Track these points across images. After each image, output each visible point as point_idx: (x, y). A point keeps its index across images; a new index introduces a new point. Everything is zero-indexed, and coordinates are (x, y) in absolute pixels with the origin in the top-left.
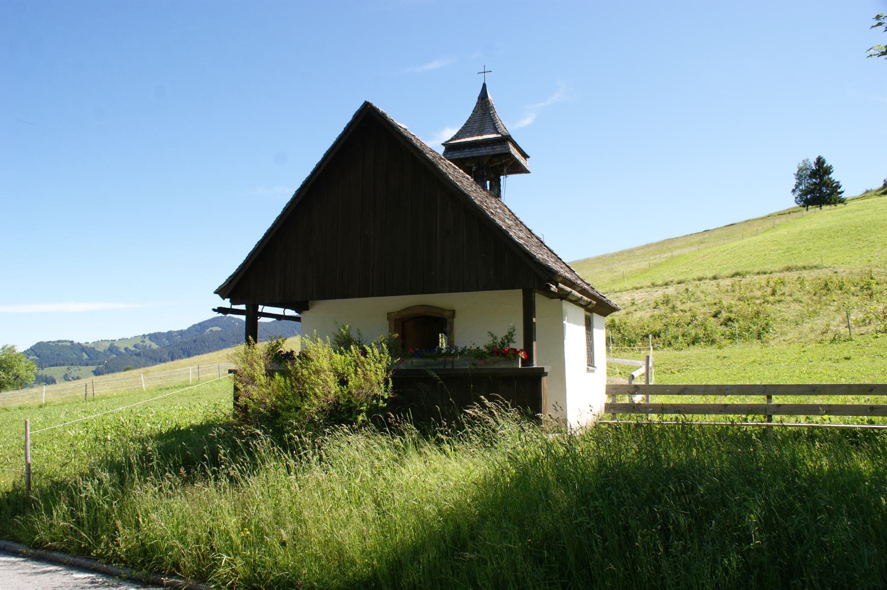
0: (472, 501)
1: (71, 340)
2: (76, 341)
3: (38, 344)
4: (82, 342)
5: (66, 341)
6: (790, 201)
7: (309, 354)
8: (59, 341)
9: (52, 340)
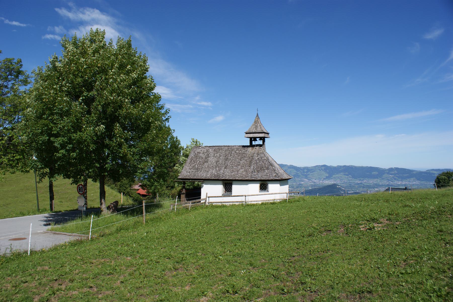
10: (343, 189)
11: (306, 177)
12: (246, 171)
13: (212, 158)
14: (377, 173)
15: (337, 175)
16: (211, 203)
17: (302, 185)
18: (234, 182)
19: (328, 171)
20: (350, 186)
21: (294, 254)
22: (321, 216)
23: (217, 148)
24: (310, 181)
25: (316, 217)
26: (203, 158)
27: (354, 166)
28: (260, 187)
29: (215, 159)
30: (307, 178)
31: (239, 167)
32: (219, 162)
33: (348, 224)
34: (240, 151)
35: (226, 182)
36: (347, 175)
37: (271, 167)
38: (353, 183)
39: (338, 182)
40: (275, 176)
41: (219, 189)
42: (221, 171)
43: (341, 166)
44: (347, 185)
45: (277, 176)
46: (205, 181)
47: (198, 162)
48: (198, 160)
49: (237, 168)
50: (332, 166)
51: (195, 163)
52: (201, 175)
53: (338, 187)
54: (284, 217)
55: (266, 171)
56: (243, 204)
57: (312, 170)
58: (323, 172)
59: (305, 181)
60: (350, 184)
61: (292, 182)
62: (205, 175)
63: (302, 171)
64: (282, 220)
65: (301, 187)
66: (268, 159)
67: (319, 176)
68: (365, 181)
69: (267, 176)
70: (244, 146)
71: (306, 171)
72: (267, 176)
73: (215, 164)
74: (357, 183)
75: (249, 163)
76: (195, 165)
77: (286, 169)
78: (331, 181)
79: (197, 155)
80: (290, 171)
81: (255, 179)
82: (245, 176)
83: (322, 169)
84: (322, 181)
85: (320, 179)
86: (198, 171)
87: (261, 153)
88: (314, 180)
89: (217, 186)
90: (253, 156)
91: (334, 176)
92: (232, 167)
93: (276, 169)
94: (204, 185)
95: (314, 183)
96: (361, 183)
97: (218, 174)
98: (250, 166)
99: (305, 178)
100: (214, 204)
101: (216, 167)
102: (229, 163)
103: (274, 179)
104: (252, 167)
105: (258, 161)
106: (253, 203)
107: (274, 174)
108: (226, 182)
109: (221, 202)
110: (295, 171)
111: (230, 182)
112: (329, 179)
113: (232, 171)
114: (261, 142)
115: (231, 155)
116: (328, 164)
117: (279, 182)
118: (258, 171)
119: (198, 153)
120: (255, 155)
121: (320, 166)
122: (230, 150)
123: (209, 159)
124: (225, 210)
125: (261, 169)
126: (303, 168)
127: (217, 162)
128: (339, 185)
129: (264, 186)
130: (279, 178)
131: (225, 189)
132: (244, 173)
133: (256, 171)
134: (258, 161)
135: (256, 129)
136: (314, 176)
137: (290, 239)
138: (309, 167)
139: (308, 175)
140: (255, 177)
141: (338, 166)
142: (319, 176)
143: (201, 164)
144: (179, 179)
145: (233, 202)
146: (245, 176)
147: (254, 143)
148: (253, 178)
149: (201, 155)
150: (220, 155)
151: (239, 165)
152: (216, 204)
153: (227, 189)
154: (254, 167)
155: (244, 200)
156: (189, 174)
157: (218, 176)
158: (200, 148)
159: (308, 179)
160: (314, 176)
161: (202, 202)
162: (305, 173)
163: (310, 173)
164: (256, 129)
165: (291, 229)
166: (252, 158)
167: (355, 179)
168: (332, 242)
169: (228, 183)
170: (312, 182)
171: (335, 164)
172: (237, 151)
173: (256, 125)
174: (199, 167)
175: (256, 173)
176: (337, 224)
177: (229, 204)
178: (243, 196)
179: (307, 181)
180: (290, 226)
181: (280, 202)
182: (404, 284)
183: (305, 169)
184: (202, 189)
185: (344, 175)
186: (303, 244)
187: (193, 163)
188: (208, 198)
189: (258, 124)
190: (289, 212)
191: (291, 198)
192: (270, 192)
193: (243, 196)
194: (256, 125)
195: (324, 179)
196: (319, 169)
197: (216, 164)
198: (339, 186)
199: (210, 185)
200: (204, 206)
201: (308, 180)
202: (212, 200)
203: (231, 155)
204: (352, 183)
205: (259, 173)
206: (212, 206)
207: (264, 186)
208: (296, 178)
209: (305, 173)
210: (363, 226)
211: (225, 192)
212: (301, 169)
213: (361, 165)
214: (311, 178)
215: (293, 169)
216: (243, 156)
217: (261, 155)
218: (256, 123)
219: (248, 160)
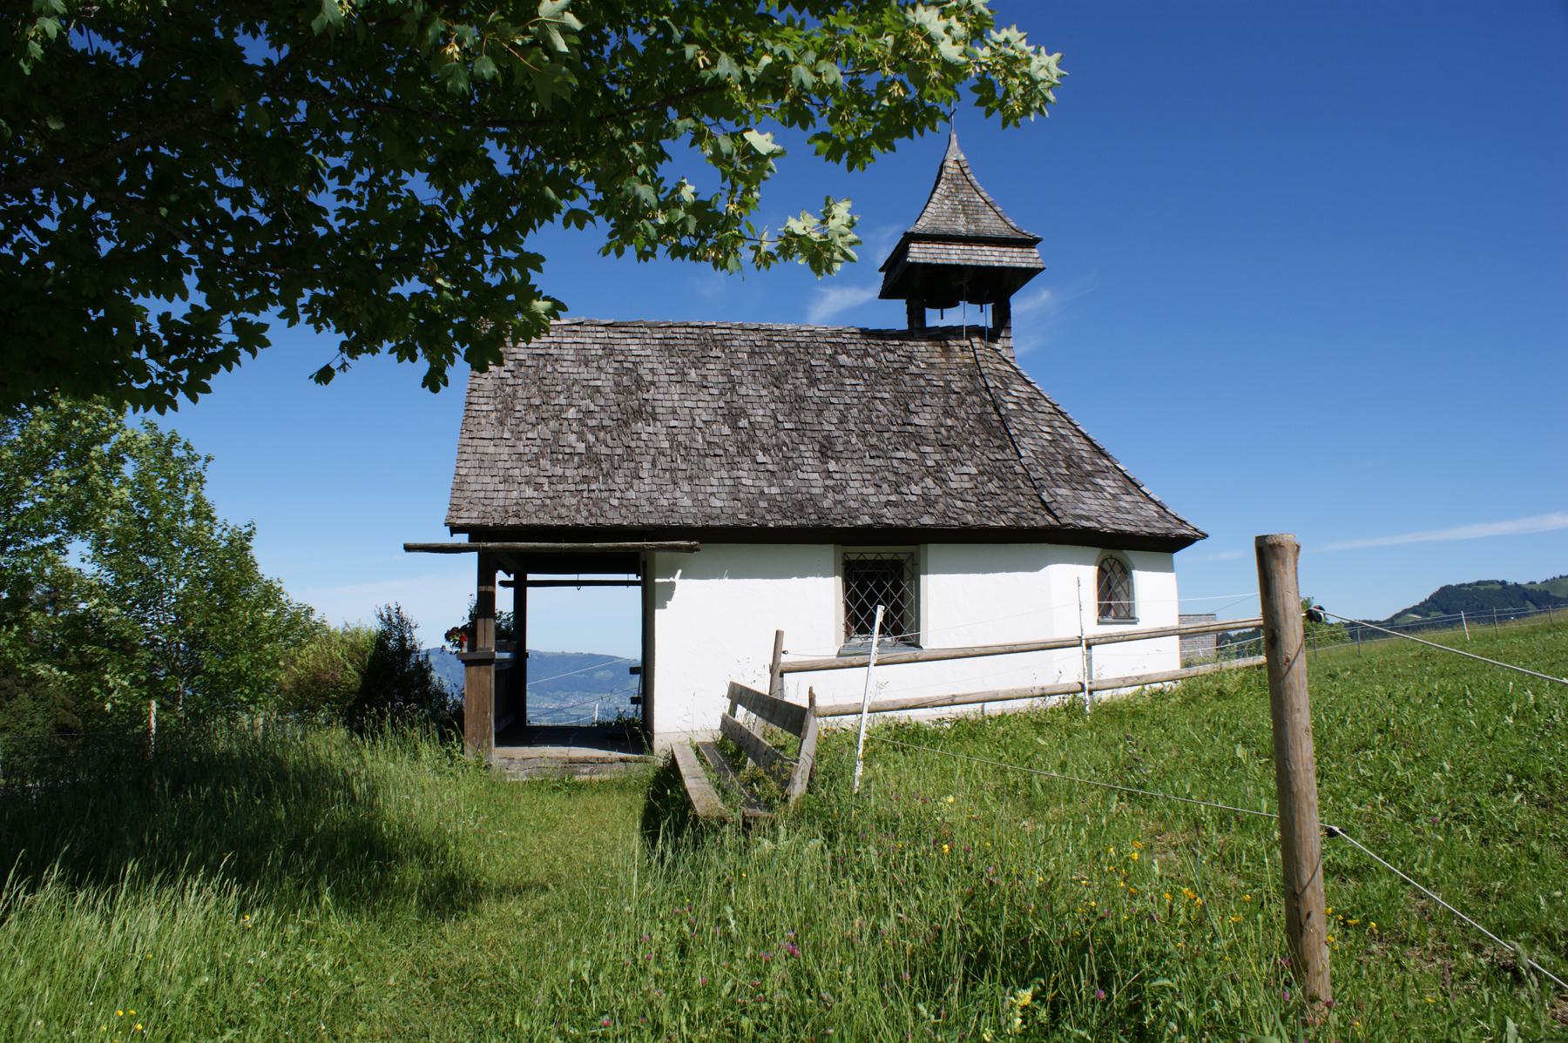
0: (965, 905)
1: (1500, 579)
2: (1511, 580)
3: (1443, 589)
4: (1523, 581)
5: (1492, 582)
6: (1304, 595)
7: (1298, 715)
8: (1479, 583)
9: (1467, 582)
14: (611, 675)
18: (933, 552)
35: (871, 553)
46: (710, 552)
68: (572, 702)
94: (677, 579)
96: (560, 710)
108: (871, 553)
111: (887, 552)
145: (952, 702)
192: (1143, 625)
199: (733, 576)
213: (559, 651)
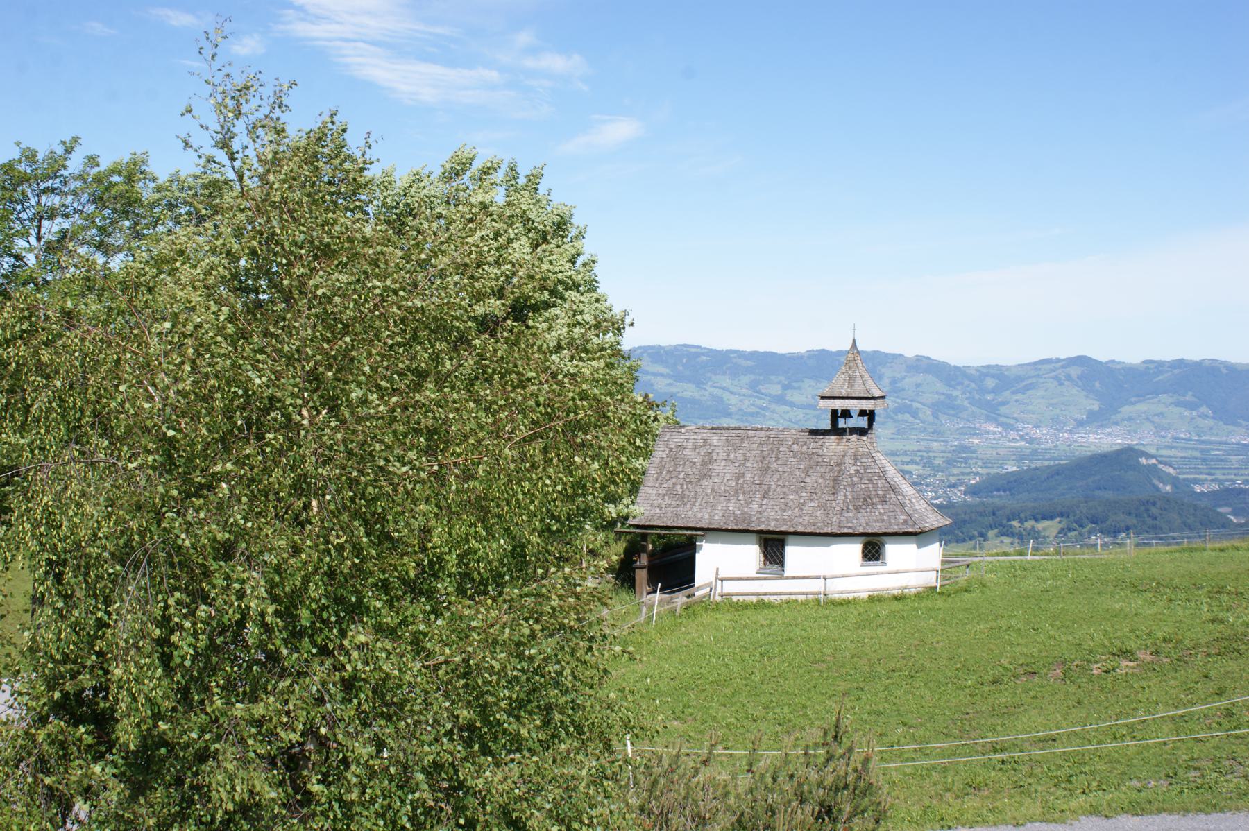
10: (1171, 470)
11: (992, 411)
12: (824, 507)
13: (723, 464)
15: (1142, 407)
16: (728, 594)
17: (974, 452)
18: (790, 539)
19: (1097, 384)
20: (1204, 460)
21: (968, 711)
22: (1020, 641)
23: (733, 433)
24: (1012, 434)
25: (1011, 644)
26: (694, 463)
27: (1222, 362)
28: (863, 552)
29: (731, 467)
30: (996, 420)
31: (804, 494)
32: (743, 476)
33: (1072, 661)
34: (802, 446)
35: (765, 536)
36: (1192, 406)
37: (893, 495)
38: (1220, 443)
39: (1145, 439)
40: (906, 522)
41: (749, 554)
42: (751, 506)
43: (1160, 364)
44: (1189, 453)
45: (911, 523)
46: (709, 534)
47: (682, 475)
48: (680, 469)
49: (797, 497)
50: (1119, 363)
51: (674, 480)
52: (695, 516)
53: (1143, 461)
54: (938, 642)
55: (880, 507)
56: (818, 601)
57: (1019, 379)
58: (1074, 391)
59: (988, 432)
60: (1202, 451)
61: (922, 436)
62: (707, 516)
63: (973, 385)
64: (935, 649)
65: (965, 461)
66: (884, 473)
67: (1058, 411)
69: (883, 521)
70: (814, 432)
71: (990, 383)
72: (883, 521)
73: (734, 484)
74: (1238, 444)
75: (831, 484)
76: (674, 484)
77: (899, 376)
78: (1110, 434)
79: (677, 452)
80: (918, 385)
81: (851, 531)
82: (823, 522)
83: (1069, 377)
84: (1071, 432)
85: (1058, 423)
86: (685, 504)
87: (863, 455)
88: (1029, 429)
89: (742, 546)
90: (841, 464)
91: (1126, 410)
92: (784, 493)
93: (908, 502)
94: (703, 543)
95: (1031, 441)
97: (743, 513)
98: (834, 494)
99: (989, 419)
100: (735, 599)
101: (736, 493)
102: (772, 481)
103: (901, 531)
104: (841, 497)
105: (855, 479)
106: (844, 596)
107: (902, 517)
109: (758, 594)
110: (940, 386)
112: (1102, 426)
113: (783, 507)
114: (863, 422)
115: (777, 459)
116: (1101, 355)
117: (913, 538)
118: (857, 508)
119: (677, 446)
120: (848, 460)
121: (1058, 360)
122: (773, 443)
123: (715, 466)
124: (762, 618)
125: (865, 501)
126: (977, 369)
127: (738, 478)
128: (1153, 451)
129: (873, 548)
130: (916, 529)
131: (765, 556)
132: (818, 513)
133: (851, 507)
134: (855, 479)
135: (851, 386)
136: (1030, 407)
137: (957, 688)
138: (1008, 368)
139: (1004, 403)
140: (850, 525)
141: (1145, 362)
142: (1058, 411)
143: (690, 482)
144: (631, 525)
146: (823, 522)
147: (842, 423)
148: (844, 527)
149: (687, 453)
150: (744, 455)
151: (803, 488)
152: (741, 598)
153: (772, 557)
154: (845, 496)
155: (822, 590)
156: (658, 511)
157: (745, 519)
158: (683, 430)
159: (1001, 424)
160: (1030, 407)
161: (698, 594)
162: (989, 397)
163: (1013, 393)
164: (851, 386)
165: (957, 669)
166: (837, 468)
167: (1231, 428)
168: (1032, 693)
169: (772, 540)
170: (1022, 438)
171: (1132, 355)
172: (795, 447)
173: (850, 372)
174: (687, 493)
175: (851, 515)
176: (1050, 660)
177: (778, 598)
178: (818, 577)
179: (995, 433)
180: (955, 664)
181: (918, 595)
182: (274, 269)
183: (987, 375)
184: (697, 555)
185: (1178, 404)
186: (982, 696)
187: (667, 478)
188: (719, 582)
189: (854, 372)
190: (948, 629)
191: (948, 582)
193: (818, 577)
194: (850, 372)
195: (1080, 423)
196: (1056, 378)
197: (737, 483)
198: (1148, 456)
200: (708, 605)
201: (1000, 429)
202: (729, 587)
203: (777, 459)
204: (1210, 443)
205: (860, 515)
206: (732, 606)
207: (873, 548)
208: (943, 418)
209: (989, 397)
210: (1099, 665)
211: (765, 564)
212: (972, 379)
214: (1016, 419)
215: (930, 377)
216: (812, 463)
217: (864, 460)
218: (850, 368)
219: (827, 476)
